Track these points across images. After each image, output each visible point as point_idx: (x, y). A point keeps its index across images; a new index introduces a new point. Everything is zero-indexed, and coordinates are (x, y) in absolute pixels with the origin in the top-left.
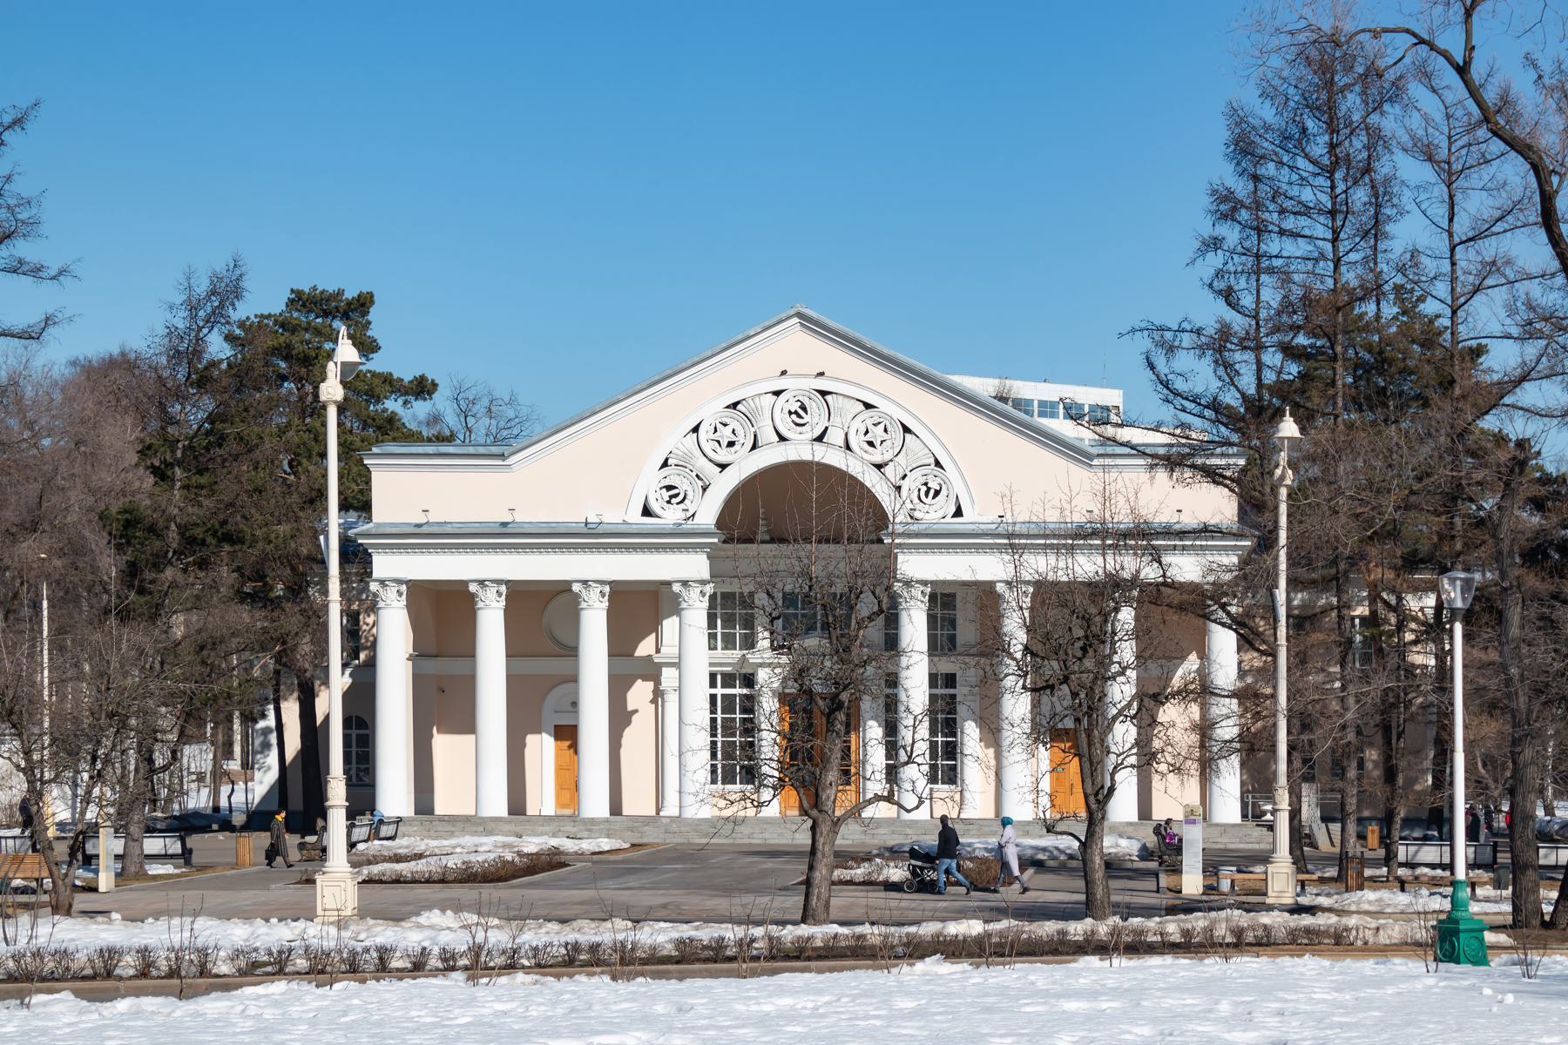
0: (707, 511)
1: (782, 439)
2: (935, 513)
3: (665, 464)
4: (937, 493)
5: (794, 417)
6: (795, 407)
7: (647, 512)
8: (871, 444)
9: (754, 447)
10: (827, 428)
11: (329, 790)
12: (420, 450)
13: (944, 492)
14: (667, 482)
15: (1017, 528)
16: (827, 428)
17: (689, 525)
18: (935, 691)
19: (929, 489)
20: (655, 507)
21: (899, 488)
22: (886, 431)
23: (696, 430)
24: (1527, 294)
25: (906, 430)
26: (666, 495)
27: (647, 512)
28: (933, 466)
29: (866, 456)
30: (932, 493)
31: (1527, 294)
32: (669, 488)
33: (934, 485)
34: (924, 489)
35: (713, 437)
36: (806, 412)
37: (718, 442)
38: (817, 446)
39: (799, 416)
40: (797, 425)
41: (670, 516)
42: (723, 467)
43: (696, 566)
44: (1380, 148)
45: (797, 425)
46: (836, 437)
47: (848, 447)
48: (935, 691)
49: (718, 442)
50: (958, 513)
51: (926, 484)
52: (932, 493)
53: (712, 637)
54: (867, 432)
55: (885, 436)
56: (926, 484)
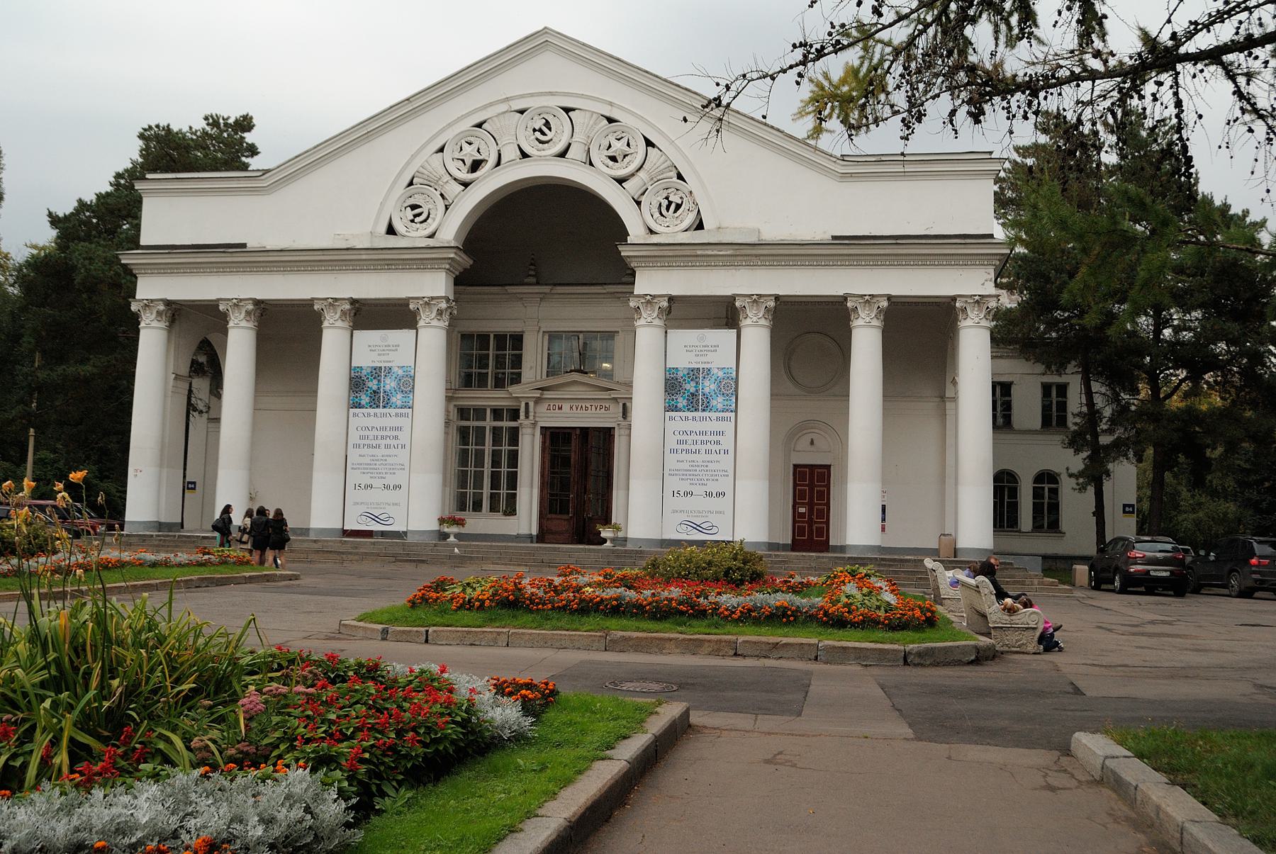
1: (524, 155)
2: (673, 230)
3: (411, 184)
4: (547, 124)
5: (538, 134)
6: (539, 124)
7: (391, 230)
8: (613, 159)
9: (498, 164)
10: (499, 151)
11: (406, 330)
15: (1084, 401)
16: (499, 151)
17: (431, 242)
19: (670, 203)
20: (398, 226)
21: (639, 203)
22: (628, 145)
23: (441, 150)
25: (479, 125)
27: (391, 230)
28: (675, 179)
29: (543, 153)
32: (414, 207)
33: (539, 124)
34: (665, 203)
36: (675, 212)
37: (463, 161)
39: (543, 133)
41: (413, 235)
42: (466, 185)
43: (436, 285)
46: (510, 153)
47: (591, 164)
49: (463, 161)
50: (700, 226)
51: (667, 198)
53: (811, 53)
54: (610, 146)
55: (474, 147)
56: (534, 130)
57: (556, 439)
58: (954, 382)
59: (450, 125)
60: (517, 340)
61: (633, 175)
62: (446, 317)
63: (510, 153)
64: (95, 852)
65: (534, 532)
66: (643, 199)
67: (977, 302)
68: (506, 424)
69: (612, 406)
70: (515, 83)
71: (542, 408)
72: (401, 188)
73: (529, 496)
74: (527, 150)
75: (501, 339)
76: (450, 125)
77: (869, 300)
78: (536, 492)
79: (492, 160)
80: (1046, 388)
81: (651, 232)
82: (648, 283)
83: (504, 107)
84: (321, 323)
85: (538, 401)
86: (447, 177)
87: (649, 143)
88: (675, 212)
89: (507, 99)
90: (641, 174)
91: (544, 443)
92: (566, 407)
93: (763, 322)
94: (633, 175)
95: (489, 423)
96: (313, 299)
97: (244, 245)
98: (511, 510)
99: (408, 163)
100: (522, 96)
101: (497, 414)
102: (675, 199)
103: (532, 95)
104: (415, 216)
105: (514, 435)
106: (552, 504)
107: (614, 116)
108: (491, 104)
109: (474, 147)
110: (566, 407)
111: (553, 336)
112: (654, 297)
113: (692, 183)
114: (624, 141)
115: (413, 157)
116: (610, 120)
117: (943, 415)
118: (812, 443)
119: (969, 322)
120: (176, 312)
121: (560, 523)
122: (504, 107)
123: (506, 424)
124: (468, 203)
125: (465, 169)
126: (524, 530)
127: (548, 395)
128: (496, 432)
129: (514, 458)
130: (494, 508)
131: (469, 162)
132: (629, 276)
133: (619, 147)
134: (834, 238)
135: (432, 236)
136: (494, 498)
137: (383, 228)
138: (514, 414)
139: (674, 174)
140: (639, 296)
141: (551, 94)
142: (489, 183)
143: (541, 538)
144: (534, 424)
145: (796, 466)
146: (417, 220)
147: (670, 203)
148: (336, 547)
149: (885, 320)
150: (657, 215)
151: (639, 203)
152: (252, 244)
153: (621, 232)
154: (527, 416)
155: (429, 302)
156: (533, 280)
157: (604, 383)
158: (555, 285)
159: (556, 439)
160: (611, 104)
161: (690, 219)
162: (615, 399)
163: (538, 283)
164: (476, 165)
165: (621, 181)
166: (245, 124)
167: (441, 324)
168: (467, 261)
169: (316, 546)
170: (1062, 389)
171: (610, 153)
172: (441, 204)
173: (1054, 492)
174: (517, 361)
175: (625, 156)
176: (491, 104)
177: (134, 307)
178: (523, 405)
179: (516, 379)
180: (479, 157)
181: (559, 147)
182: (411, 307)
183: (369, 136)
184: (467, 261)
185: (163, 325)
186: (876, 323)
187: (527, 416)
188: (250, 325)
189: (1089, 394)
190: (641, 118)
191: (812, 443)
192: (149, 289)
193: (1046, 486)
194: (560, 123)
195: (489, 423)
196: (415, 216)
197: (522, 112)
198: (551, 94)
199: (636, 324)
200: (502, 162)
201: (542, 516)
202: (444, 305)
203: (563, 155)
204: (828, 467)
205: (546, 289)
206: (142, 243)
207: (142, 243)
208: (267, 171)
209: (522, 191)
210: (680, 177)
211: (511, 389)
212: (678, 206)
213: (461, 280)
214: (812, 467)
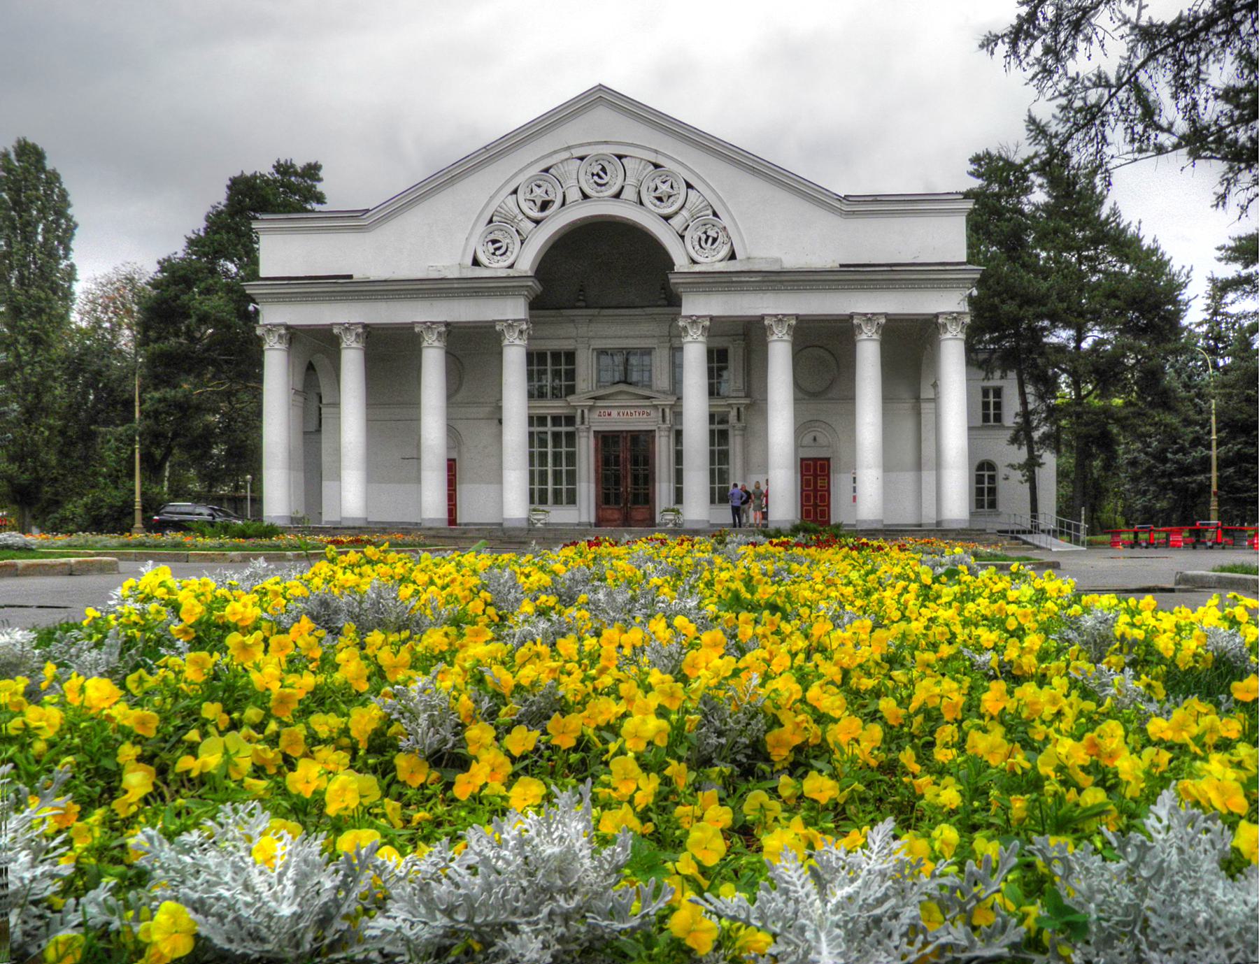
0: (526, 260)
1: (585, 196)
2: (712, 260)
3: (491, 221)
4: (604, 169)
5: (596, 178)
6: (597, 169)
7: (476, 262)
8: (660, 199)
9: (563, 204)
12: (304, 215)
13: (606, 164)
14: (492, 237)
17: (511, 272)
18: (532, 429)
19: (708, 237)
20: (483, 258)
21: (682, 237)
23: (515, 192)
24: (1222, 198)
26: (491, 248)
27: (476, 262)
30: (602, 174)
31: (1222, 198)
32: (494, 242)
33: (597, 169)
34: (704, 237)
35: (529, 197)
36: (713, 244)
38: (616, 202)
39: (600, 177)
40: (599, 185)
41: (496, 267)
42: (537, 222)
43: (514, 309)
44: (1117, 135)
45: (599, 185)
46: (629, 193)
47: (641, 203)
48: (532, 429)
50: (732, 256)
52: (602, 174)
55: (543, 189)
57: (606, 440)
58: (935, 386)
59: (521, 170)
60: (571, 356)
61: (676, 213)
62: (525, 336)
63: (574, 195)
64: (1256, 810)
65: (593, 520)
66: (687, 234)
67: (955, 318)
68: (563, 429)
69: (653, 413)
70: (573, 134)
71: (595, 415)
72: (482, 227)
73: (586, 489)
74: (588, 191)
75: (556, 356)
76: (521, 170)
77: (780, 319)
78: (593, 486)
79: (558, 202)
80: (985, 392)
81: (694, 262)
82: (696, 306)
83: (566, 155)
84: (420, 343)
85: (591, 408)
86: (521, 216)
87: (689, 186)
88: (713, 244)
89: (569, 148)
90: (684, 212)
91: (596, 445)
92: (614, 413)
93: (786, 337)
94: (676, 213)
95: (550, 428)
96: (413, 323)
97: (350, 277)
98: (572, 500)
99: (487, 204)
100: (582, 145)
101: (556, 420)
102: (712, 233)
103: (589, 144)
104: (497, 249)
105: (571, 437)
106: (608, 496)
107: (660, 161)
108: (555, 152)
109: (543, 189)
110: (614, 413)
111: (602, 352)
112: (699, 317)
113: (725, 220)
114: (669, 184)
115: (492, 198)
116: (657, 166)
117: (918, 414)
118: (815, 439)
119: (948, 335)
120: (294, 336)
121: (639, 513)
122: (566, 155)
123: (563, 429)
124: (540, 239)
125: (536, 209)
126: (584, 519)
127: (599, 403)
128: (556, 436)
129: (571, 458)
130: (557, 501)
131: (539, 203)
132: (674, 301)
133: (664, 188)
134: (841, 266)
135: (511, 266)
136: (557, 493)
137: (469, 261)
138: (570, 420)
139: (710, 212)
140: (686, 317)
141: (606, 143)
142: (557, 221)
143: (599, 522)
144: (588, 429)
145: (802, 460)
146: (498, 253)
147: (708, 237)
148: (448, 533)
149: (882, 335)
150: (697, 247)
151: (682, 237)
152: (358, 276)
153: (670, 264)
154: (583, 423)
155: (511, 325)
156: (583, 304)
157: (647, 393)
158: (602, 308)
159: (606, 440)
160: (656, 152)
161: (724, 251)
162: (656, 407)
163: (587, 307)
164: (545, 206)
165: (667, 218)
166: (312, 171)
167: (522, 343)
168: (538, 288)
169: (432, 533)
170: (998, 392)
171: (657, 194)
172: (517, 239)
173: (992, 479)
174: (571, 375)
175: (670, 197)
176: (555, 152)
177: (259, 332)
178: (579, 412)
179: (571, 390)
180: (547, 198)
181: (614, 189)
182: (498, 328)
183: (754, 171)
184: (538, 288)
185: (283, 346)
186: (875, 337)
187: (583, 423)
188: (360, 346)
189: (1023, 394)
190: (682, 164)
191: (815, 439)
192: (272, 315)
193: (986, 473)
194: (614, 168)
195: (550, 428)
196: (497, 249)
197: (582, 159)
198: (606, 143)
199: (684, 340)
200: (568, 201)
201: (598, 507)
202: (524, 327)
203: (617, 196)
204: (828, 460)
205: (595, 311)
206: (262, 274)
207: (262, 274)
208: (367, 211)
209: (587, 225)
210: (715, 214)
211: (569, 399)
212: (715, 240)
213: (535, 305)
214: (815, 460)
